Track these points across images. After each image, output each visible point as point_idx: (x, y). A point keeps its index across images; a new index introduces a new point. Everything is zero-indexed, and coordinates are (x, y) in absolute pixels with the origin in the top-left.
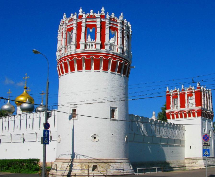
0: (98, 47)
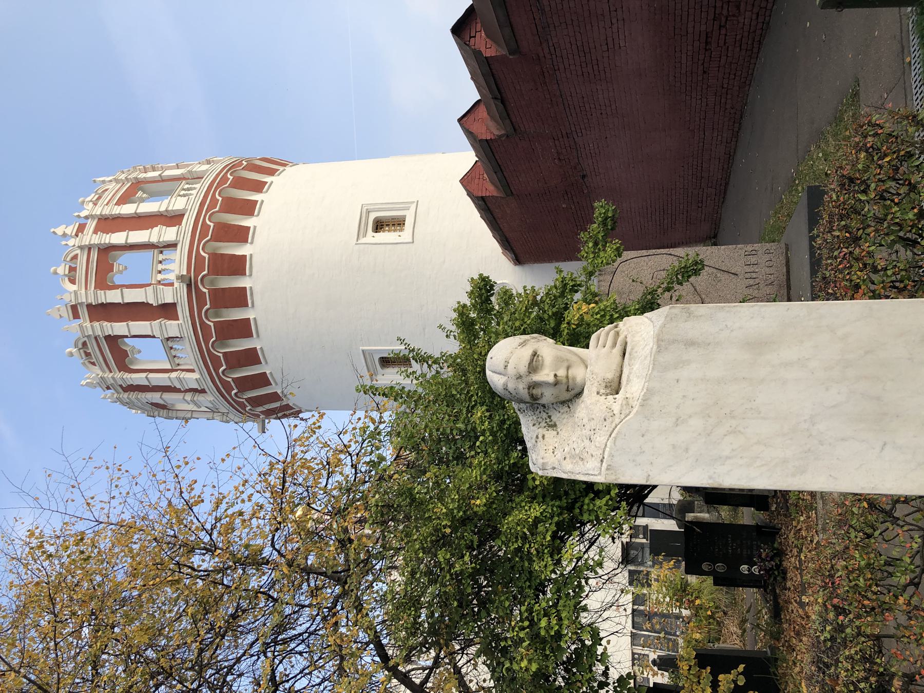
0: (169, 234)
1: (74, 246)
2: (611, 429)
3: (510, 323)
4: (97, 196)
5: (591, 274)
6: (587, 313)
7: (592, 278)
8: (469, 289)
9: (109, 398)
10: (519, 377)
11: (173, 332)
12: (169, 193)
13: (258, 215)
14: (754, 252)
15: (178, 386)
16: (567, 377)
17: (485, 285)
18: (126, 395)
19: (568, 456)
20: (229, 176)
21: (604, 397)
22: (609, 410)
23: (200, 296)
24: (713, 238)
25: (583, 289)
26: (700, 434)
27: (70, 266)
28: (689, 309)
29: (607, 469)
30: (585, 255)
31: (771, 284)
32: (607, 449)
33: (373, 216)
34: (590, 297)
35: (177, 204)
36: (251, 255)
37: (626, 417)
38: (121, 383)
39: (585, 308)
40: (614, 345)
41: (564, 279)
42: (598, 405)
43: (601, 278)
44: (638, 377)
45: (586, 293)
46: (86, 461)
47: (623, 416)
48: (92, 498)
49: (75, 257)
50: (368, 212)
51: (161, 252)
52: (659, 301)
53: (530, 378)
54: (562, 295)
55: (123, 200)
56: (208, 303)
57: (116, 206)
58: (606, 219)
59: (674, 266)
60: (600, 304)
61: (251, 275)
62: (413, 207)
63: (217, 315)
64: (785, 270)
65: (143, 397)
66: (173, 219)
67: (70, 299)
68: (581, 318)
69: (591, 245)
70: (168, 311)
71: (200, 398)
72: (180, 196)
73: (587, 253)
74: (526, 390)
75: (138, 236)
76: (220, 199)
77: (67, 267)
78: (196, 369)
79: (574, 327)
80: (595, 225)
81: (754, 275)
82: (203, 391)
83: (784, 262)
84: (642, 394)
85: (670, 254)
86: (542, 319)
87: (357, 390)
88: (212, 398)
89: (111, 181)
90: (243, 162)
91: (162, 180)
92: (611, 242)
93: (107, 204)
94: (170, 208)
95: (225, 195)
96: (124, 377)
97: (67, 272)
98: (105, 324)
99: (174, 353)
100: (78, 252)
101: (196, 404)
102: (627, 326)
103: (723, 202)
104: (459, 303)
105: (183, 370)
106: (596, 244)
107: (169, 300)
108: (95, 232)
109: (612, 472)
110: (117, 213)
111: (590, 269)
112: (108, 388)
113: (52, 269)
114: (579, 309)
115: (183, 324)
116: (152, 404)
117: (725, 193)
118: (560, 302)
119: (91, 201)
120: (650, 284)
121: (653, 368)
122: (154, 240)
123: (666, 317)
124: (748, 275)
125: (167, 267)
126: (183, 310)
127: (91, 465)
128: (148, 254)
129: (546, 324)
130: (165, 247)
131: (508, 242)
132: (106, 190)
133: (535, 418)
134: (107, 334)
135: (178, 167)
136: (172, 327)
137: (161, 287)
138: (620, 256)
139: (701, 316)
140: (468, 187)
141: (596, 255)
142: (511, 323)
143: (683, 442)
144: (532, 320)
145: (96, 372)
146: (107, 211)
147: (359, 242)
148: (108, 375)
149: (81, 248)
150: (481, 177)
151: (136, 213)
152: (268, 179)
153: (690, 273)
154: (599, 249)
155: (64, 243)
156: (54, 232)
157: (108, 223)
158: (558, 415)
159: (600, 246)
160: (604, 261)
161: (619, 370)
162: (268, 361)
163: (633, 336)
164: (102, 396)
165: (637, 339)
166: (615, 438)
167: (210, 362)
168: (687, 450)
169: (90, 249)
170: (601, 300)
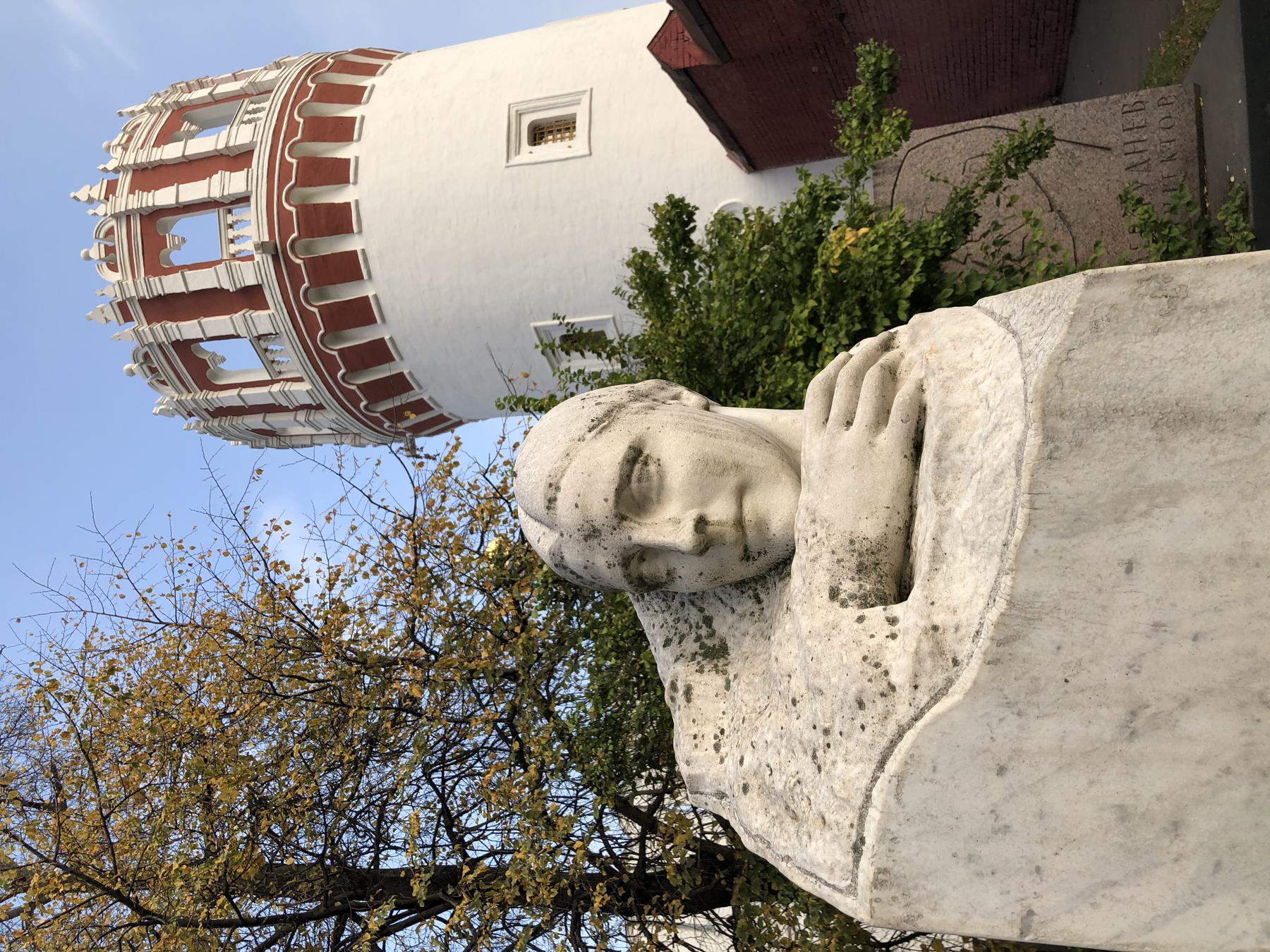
0: (235, 182)
1: (106, 215)
2: (884, 742)
3: (729, 274)
4: (126, 136)
5: (858, 175)
6: (854, 245)
7: (862, 181)
8: (653, 223)
9: (194, 428)
10: (591, 534)
11: (264, 327)
12: (227, 120)
13: (359, 138)
14: (1139, 106)
15: (285, 403)
16: (739, 523)
17: (680, 215)
18: (216, 423)
19: (753, 783)
20: (309, 83)
21: (853, 612)
22: (872, 671)
23: (293, 269)
24: (1056, 94)
25: (848, 201)
26: (1228, 771)
27: (106, 246)
28: (1168, 279)
29: (877, 884)
30: (847, 142)
31: (1171, 158)
32: (874, 815)
33: (527, 121)
34: (861, 215)
35: (241, 135)
36: (357, 202)
37: (935, 699)
38: (205, 406)
39: (850, 237)
40: (882, 416)
41: (813, 187)
42: (836, 641)
43: (879, 180)
44: (973, 548)
45: (852, 209)
46: (132, 539)
47: (922, 698)
48: (150, 591)
49: (111, 231)
50: (520, 115)
51: (230, 212)
52: (977, 210)
53: (624, 536)
54: (812, 216)
55: (165, 137)
56: (306, 280)
57: (155, 149)
58: (878, 74)
59: (1001, 147)
60: (877, 227)
61: (360, 231)
62: (586, 99)
63: (323, 296)
64: (1194, 130)
65: (240, 422)
66: (238, 158)
67: (113, 293)
68: (845, 255)
69: (855, 123)
70: (251, 297)
71: (317, 417)
72: (243, 122)
73: (850, 139)
74: (618, 571)
75: (193, 191)
76: (301, 121)
77: (102, 246)
78: (305, 377)
79: (834, 271)
80: (860, 88)
81: (1140, 146)
82: (319, 407)
83: (1193, 116)
84: (993, 615)
85: (993, 127)
86: (780, 263)
87: (498, 406)
88: (334, 416)
89: (142, 111)
90: (329, 59)
91: (215, 100)
92: (890, 114)
93: (142, 148)
94: (231, 144)
95: (308, 114)
96: (209, 397)
97: (103, 255)
98: (169, 324)
99: (270, 357)
100: (113, 223)
101: (312, 425)
102: (924, 345)
103: (1072, 32)
104: (634, 250)
105: (287, 380)
106: (864, 121)
107: (251, 281)
108: (131, 191)
109: (894, 892)
110: (158, 158)
111: (857, 165)
112: (190, 415)
113: (83, 252)
114: (841, 239)
115: (276, 314)
116: (254, 431)
117: (1074, 16)
118: (809, 231)
119: (119, 145)
120: (958, 179)
121: (1029, 521)
122: (216, 194)
123: (1073, 319)
124: (1129, 148)
125: (241, 232)
126: (272, 294)
127: (140, 543)
128: (211, 216)
130: (232, 203)
131: (736, 140)
132: (138, 126)
133: (670, 620)
134: (174, 339)
135: (235, 78)
136: (262, 320)
137: (237, 263)
138: (906, 138)
139: (1219, 306)
140: (661, 56)
141: (866, 142)
142: (729, 274)
143: (1159, 798)
145: (168, 395)
146: (142, 158)
147: (511, 163)
148: (186, 397)
149: (116, 216)
150: (680, 36)
151: (183, 156)
152: (367, 82)
153: (1030, 156)
154: (870, 129)
155: (91, 212)
156: (75, 198)
157: (148, 176)
158: (731, 619)
159: (871, 124)
160: (880, 150)
161: (902, 507)
162: (404, 356)
163: (946, 387)
164: (185, 427)
165: (959, 397)
166: (900, 778)
167: (322, 364)
168: (1176, 827)
169: (128, 217)
170: (879, 219)
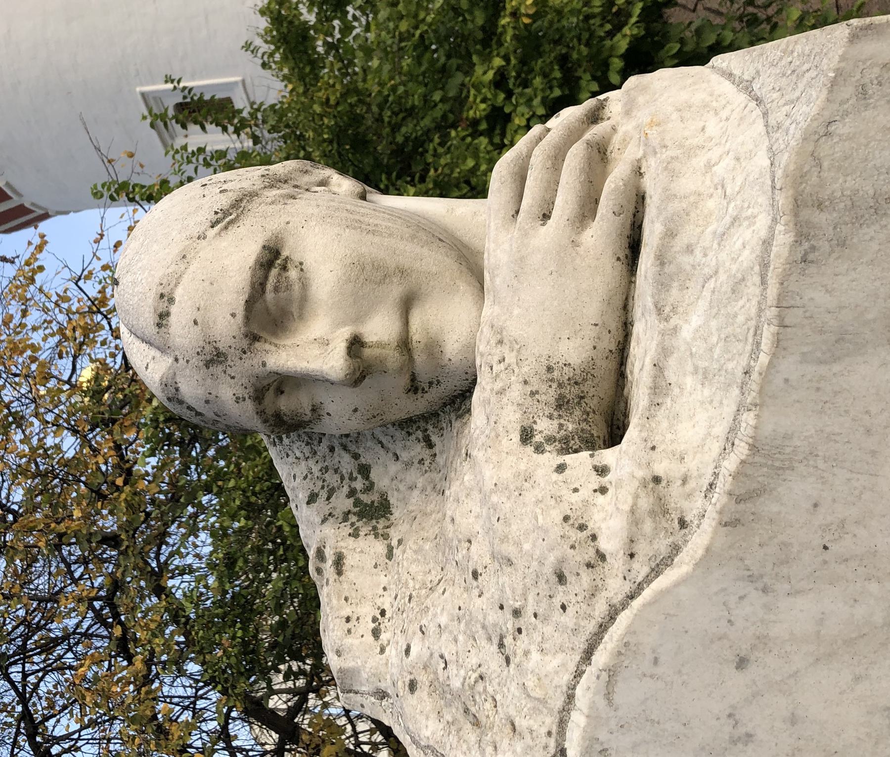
2: (591, 627)
16: (405, 344)
19: (423, 679)
21: (551, 459)
22: (576, 536)
32: (578, 720)
37: (656, 571)
42: (529, 497)
44: (706, 377)
47: (641, 569)
53: (256, 361)
74: (249, 405)
79: (527, 21)
84: (730, 464)
102: (643, 116)
121: (778, 342)
129: (465, 20)
133: (316, 469)
142: (391, 25)
144: (438, 13)
158: (394, 468)
161: (614, 324)
163: (670, 170)
165: (687, 184)
166: (611, 673)
